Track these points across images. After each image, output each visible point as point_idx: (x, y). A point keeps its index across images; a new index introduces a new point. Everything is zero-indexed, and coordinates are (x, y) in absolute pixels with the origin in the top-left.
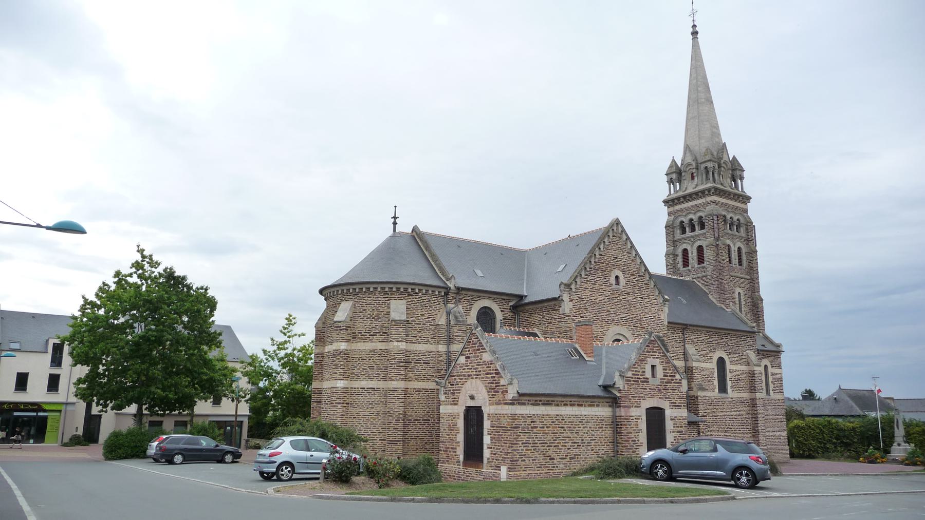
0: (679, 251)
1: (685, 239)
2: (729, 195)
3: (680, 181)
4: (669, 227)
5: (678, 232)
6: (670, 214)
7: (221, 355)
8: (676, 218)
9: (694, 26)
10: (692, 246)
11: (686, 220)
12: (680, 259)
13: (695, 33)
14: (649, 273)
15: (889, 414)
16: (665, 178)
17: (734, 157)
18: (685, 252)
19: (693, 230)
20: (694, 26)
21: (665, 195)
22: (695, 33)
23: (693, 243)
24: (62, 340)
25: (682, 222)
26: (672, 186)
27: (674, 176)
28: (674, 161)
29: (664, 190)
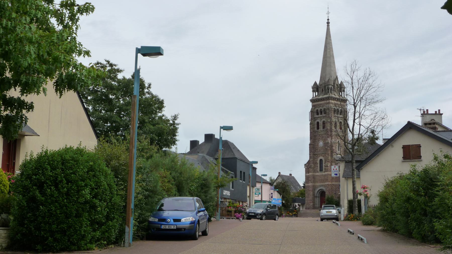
0: (316, 122)
1: (319, 117)
2: (335, 99)
3: (318, 92)
4: (312, 112)
5: (315, 114)
6: (313, 106)
7: (402, 201)
8: (315, 108)
9: (328, 20)
10: (321, 121)
11: (319, 109)
12: (316, 126)
13: (328, 23)
14: (76, 90)
15: (73, 171)
16: (311, 89)
17: (341, 82)
18: (318, 123)
19: (321, 114)
20: (328, 20)
21: (311, 97)
22: (328, 23)
23: (321, 120)
24: (91, 201)
25: (321, 109)
26: (314, 93)
27: (315, 89)
28: (315, 83)
29: (310, 95)
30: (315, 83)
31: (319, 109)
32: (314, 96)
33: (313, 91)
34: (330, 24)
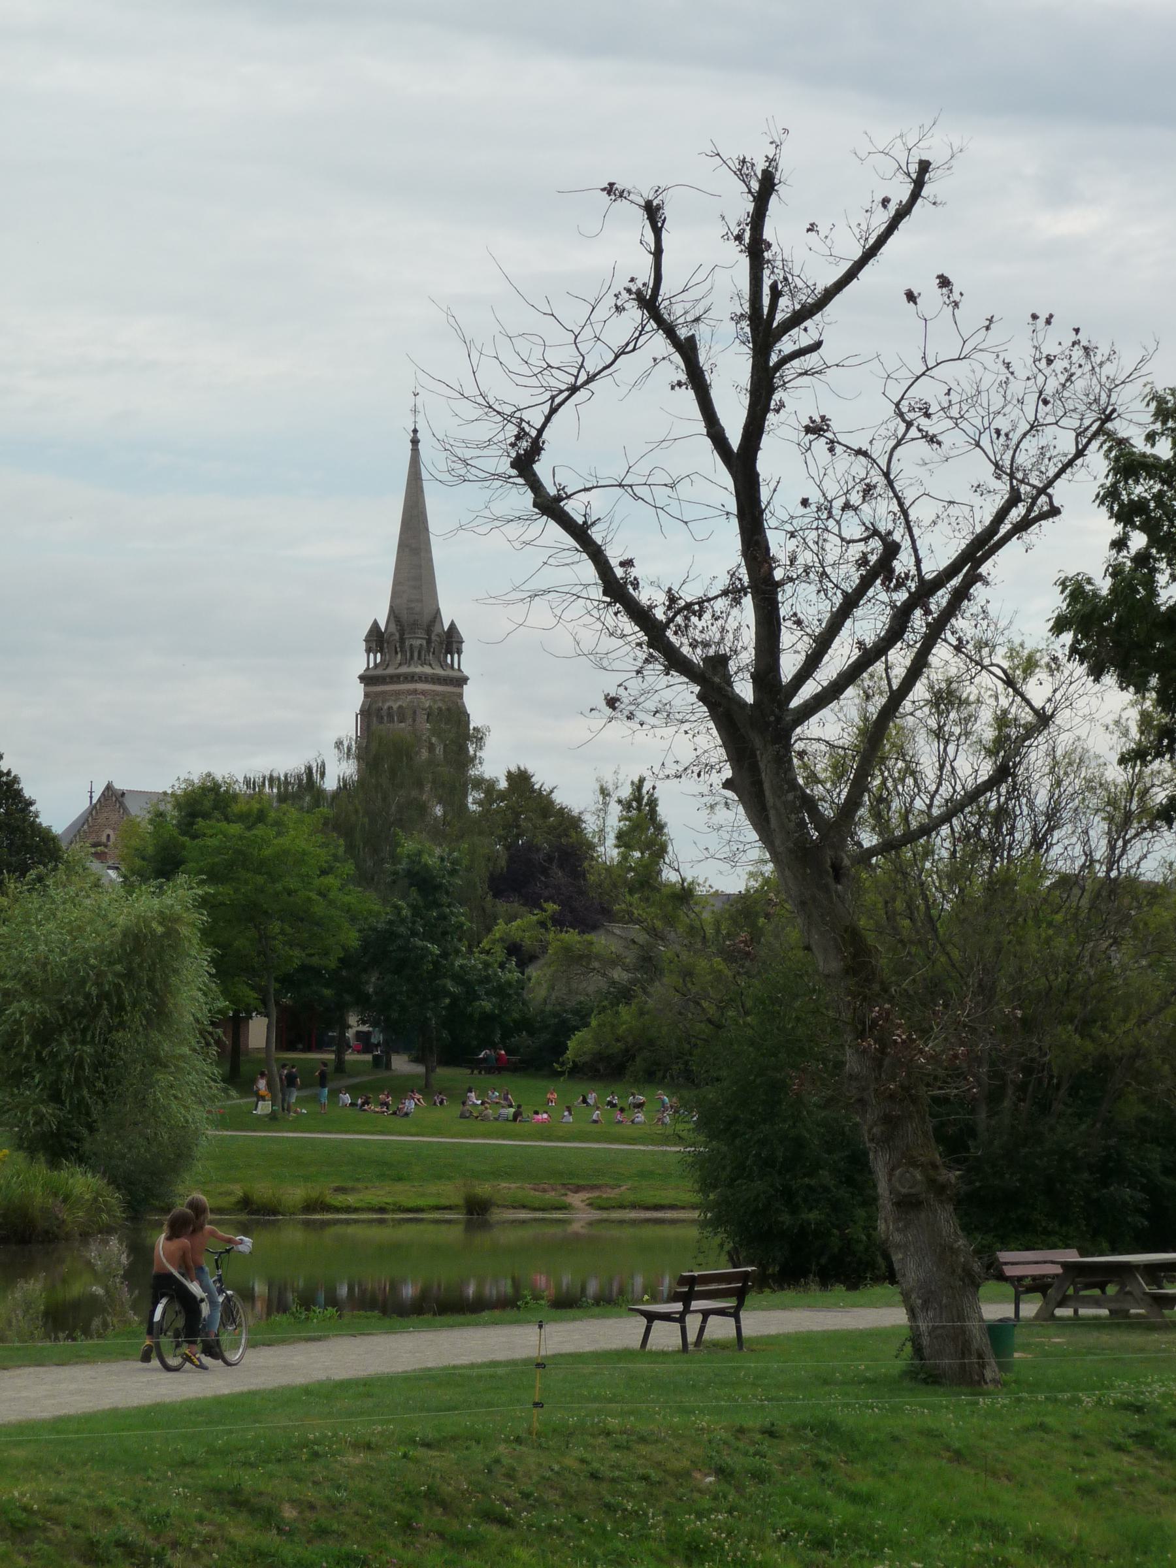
9: (415, 431)
13: (415, 442)
22: (415, 442)
30: (376, 624)
31: (395, 706)
32: (372, 665)
33: (369, 650)
34: (420, 446)
